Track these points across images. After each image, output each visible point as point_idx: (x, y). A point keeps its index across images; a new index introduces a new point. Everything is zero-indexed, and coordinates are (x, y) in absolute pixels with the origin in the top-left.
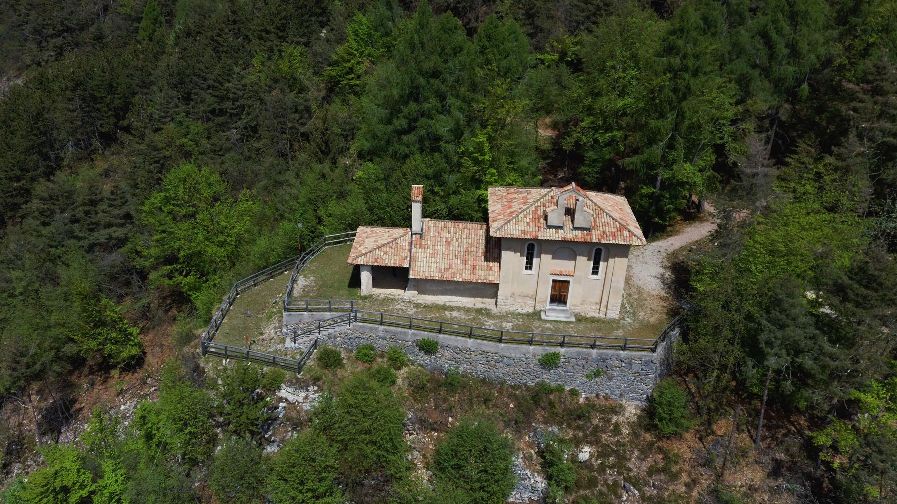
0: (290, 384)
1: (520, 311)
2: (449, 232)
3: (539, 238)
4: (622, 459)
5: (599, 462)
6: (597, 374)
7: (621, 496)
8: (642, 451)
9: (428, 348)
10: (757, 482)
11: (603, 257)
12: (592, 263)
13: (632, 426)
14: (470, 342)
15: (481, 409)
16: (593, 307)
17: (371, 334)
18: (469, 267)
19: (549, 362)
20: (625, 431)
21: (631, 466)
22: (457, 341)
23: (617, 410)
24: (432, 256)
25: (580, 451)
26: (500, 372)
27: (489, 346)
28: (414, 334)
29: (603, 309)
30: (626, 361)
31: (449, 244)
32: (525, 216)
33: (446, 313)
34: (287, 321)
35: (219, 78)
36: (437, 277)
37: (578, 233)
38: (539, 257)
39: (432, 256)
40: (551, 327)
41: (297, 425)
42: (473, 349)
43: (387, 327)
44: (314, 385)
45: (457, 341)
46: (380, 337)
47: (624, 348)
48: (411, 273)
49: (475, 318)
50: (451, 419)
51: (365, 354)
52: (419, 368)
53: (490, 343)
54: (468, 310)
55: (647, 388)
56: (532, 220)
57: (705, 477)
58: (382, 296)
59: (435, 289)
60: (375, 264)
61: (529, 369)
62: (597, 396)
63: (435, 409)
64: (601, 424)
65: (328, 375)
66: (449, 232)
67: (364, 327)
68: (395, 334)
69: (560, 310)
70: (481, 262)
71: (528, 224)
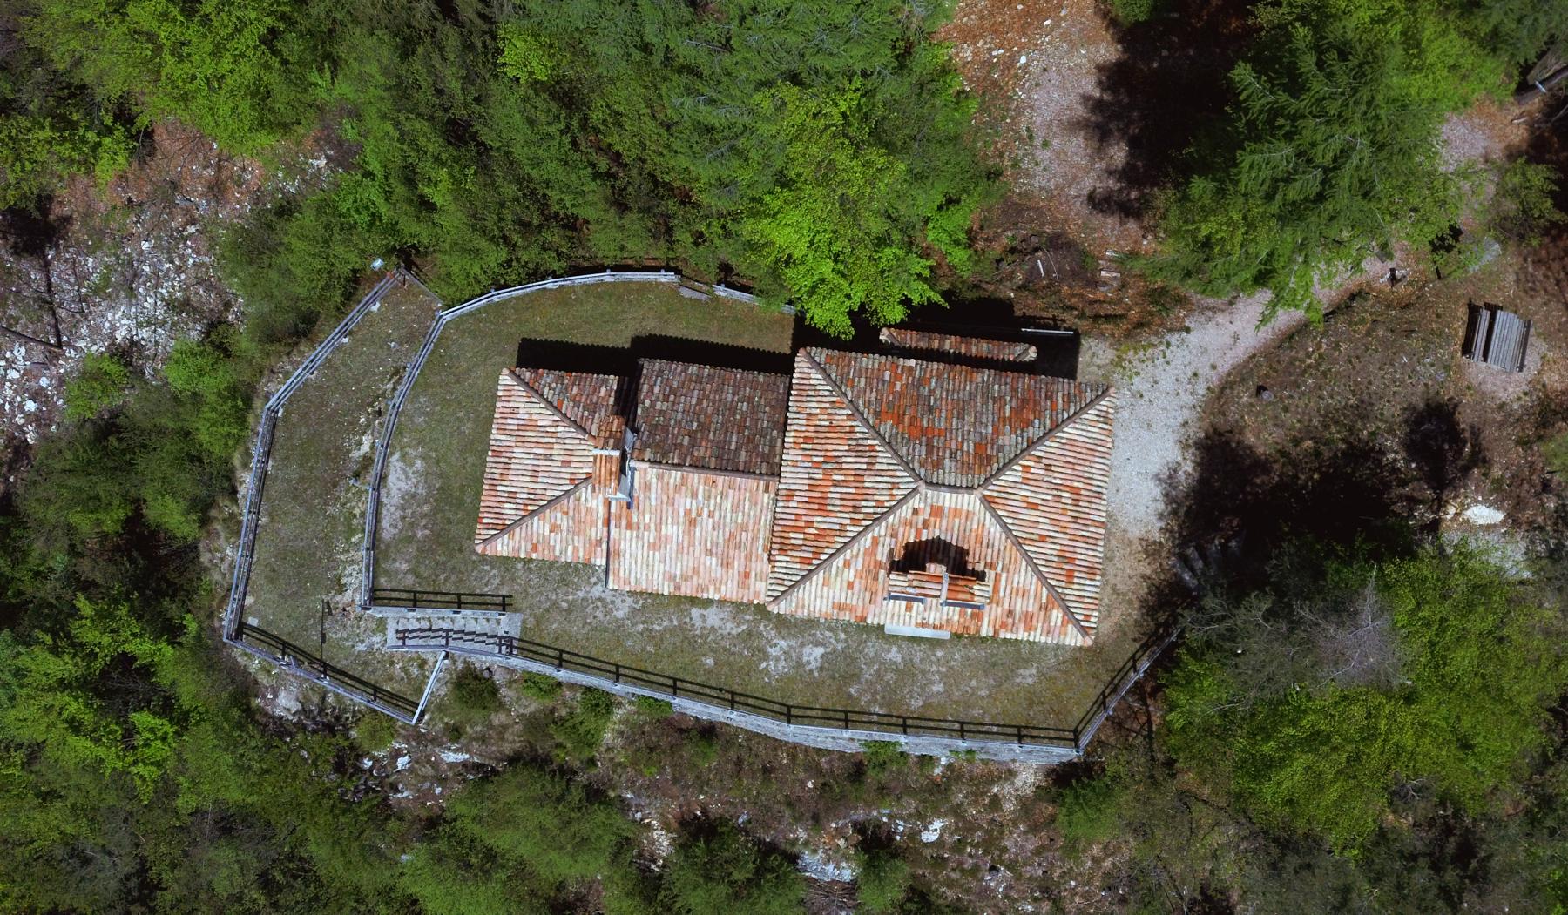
2: (694, 495)
5: (957, 837)
21: (1008, 843)
24: (654, 546)
25: (926, 828)
31: (692, 523)
32: (847, 564)
39: (654, 546)
49: (749, 634)
56: (859, 575)
66: (694, 495)
71: (850, 586)
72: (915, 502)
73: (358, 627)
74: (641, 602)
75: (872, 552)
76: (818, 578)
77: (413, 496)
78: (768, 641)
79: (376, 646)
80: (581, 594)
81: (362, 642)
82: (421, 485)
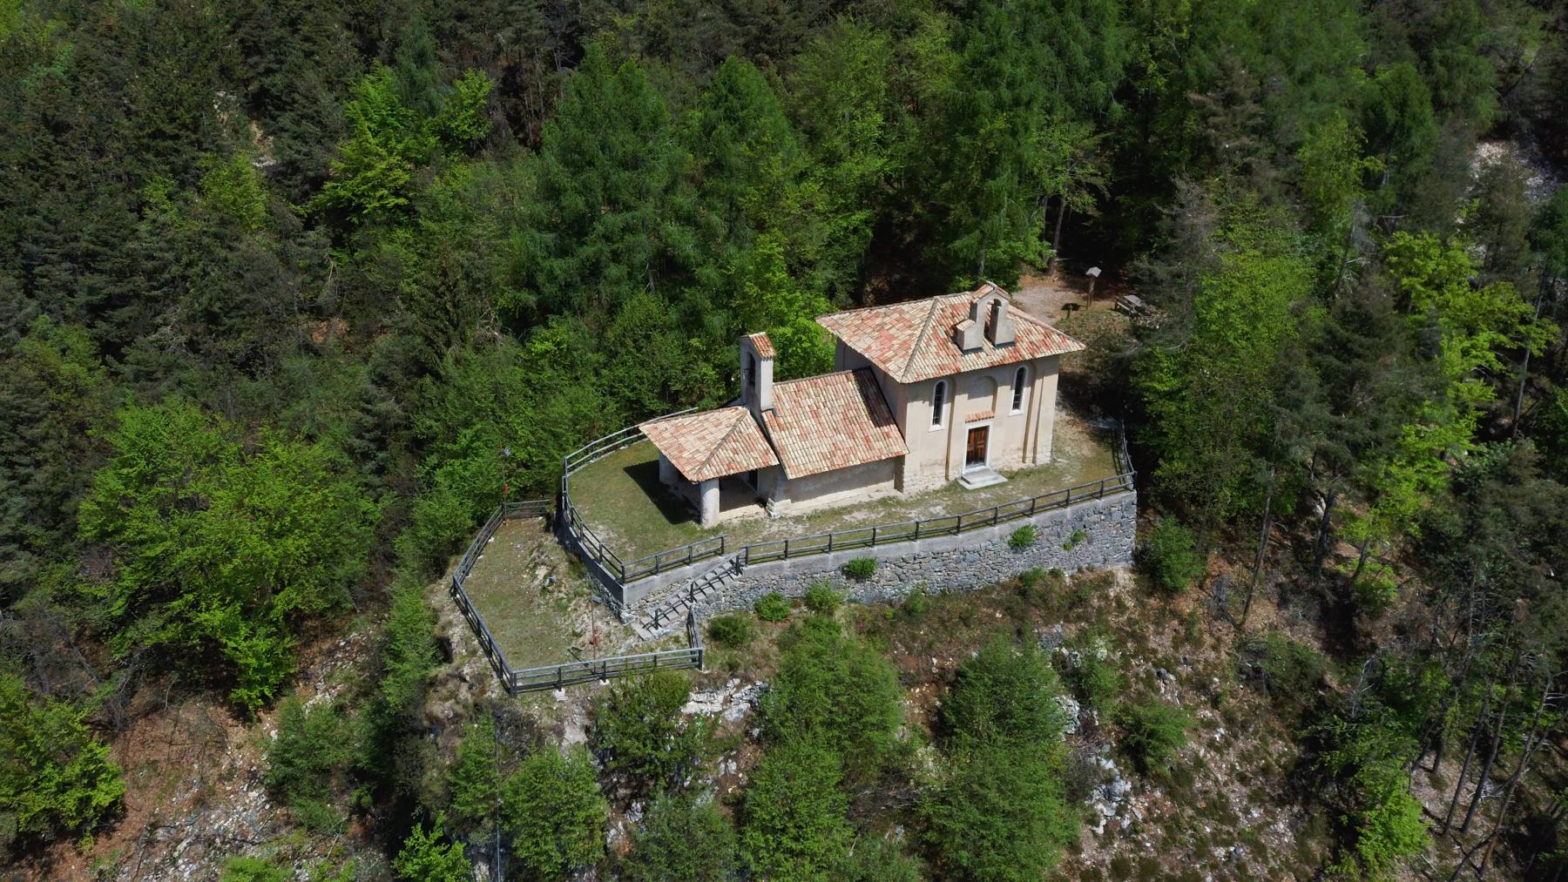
0: (701, 688)
1: (931, 488)
4: (1140, 639)
7: (1159, 689)
8: (1157, 624)
9: (858, 572)
10: (1273, 618)
11: (1026, 379)
13: (1133, 594)
14: (918, 546)
15: (964, 634)
18: (860, 441)
19: (1019, 542)
20: (1130, 603)
22: (900, 548)
23: (1107, 581)
26: (964, 576)
27: (942, 543)
28: (795, 566)
29: (1029, 454)
31: (816, 414)
32: (928, 345)
33: (845, 517)
35: (104, 236)
36: (825, 467)
38: (952, 400)
41: (729, 748)
42: (922, 555)
43: (794, 560)
44: (733, 676)
45: (900, 548)
47: (1101, 494)
48: (788, 471)
50: (935, 661)
51: (769, 609)
53: (944, 538)
54: (870, 506)
55: (1129, 542)
57: (1225, 631)
59: (812, 488)
60: (732, 472)
62: (1080, 570)
63: (910, 654)
64: (1103, 603)
67: (761, 569)
68: (809, 565)
69: (979, 472)
70: (872, 430)
72: (939, 306)
75: (935, 334)
76: (918, 358)
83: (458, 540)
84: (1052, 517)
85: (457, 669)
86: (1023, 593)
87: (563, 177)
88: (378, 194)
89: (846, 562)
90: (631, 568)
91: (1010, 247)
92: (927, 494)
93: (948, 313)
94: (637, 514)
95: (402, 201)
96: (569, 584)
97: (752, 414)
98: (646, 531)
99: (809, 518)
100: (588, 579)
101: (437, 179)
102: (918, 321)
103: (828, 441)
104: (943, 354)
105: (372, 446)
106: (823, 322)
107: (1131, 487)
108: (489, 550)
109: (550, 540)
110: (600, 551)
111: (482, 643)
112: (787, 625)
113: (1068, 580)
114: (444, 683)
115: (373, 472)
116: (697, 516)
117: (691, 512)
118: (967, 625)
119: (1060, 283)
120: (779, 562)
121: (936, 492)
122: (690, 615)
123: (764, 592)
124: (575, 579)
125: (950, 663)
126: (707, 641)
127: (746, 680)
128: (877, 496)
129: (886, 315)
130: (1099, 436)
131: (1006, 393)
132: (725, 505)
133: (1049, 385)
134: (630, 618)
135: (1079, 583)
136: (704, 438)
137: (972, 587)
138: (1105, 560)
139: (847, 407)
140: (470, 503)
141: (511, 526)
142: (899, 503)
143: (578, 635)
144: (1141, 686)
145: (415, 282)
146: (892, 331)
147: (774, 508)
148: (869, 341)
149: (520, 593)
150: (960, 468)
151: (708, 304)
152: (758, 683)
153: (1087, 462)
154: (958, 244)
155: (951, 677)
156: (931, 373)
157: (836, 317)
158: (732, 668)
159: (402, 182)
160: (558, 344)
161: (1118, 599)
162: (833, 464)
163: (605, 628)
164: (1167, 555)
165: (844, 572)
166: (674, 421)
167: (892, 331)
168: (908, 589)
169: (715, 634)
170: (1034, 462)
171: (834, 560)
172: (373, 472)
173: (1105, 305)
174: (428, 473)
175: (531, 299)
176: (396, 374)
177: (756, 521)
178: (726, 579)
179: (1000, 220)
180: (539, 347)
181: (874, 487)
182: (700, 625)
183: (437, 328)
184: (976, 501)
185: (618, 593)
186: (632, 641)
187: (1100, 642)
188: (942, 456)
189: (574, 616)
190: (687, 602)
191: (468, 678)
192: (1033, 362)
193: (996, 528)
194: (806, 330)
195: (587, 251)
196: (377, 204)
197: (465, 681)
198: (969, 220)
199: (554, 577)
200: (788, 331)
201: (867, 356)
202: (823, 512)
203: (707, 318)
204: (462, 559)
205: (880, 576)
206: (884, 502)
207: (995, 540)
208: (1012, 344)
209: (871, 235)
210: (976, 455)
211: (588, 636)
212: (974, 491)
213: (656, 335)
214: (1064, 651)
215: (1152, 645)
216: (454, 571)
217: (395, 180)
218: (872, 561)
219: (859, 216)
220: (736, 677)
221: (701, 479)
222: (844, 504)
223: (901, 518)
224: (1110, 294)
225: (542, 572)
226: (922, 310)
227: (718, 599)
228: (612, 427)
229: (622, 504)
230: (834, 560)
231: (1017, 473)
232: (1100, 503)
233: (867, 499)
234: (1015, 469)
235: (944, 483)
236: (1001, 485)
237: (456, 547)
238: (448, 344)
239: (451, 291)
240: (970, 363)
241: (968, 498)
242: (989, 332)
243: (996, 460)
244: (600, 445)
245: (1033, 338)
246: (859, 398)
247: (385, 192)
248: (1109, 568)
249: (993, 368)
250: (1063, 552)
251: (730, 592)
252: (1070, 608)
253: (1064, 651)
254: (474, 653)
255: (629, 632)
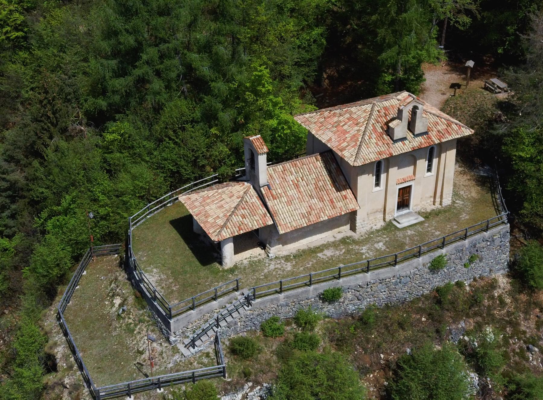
1: (375, 228)
3: (394, 154)
4: (515, 325)
6: (471, 260)
12: (427, 162)
13: (511, 294)
14: (369, 276)
15: (401, 335)
16: (429, 201)
17: (272, 306)
18: (327, 203)
20: (508, 301)
22: (357, 279)
23: (493, 285)
26: (401, 293)
27: (385, 273)
28: (287, 297)
29: (438, 200)
30: (490, 240)
31: (297, 186)
32: (370, 138)
33: (320, 255)
34: (174, 329)
36: (304, 223)
37: (420, 139)
38: (387, 171)
40: (413, 232)
42: (372, 281)
44: (248, 381)
46: (282, 306)
47: (487, 229)
50: (382, 356)
52: (326, 319)
54: (334, 245)
55: (505, 257)
56: (376, 138)
58: (245, 262)
60: (242, 232)
61: (423, 280)
62: (475, 279)
65: (252, 366)
68: (297, 296)
69: (405, 214)
72: (376, 108)
73: (163, 358)
74: (294, 262)
75: (375, 129)
76: (364, 146)
77: (161, 280)
78: (359, 249)
79: (178, 360)
80: (266, 271)
81: (169, 363)
82: (162, 276)
83: (63, 276)
84: (456, 247)
85: (60, 380)
86: (439, 302)
87: (119, 24)
88: (4, 30)
89: (321, 291)
90: (173, 303)
91: (417, 54)
92: (372, 233)
93: (382, 113)
94: (178, 259)
95: (20, 34)
96: (135, 313)
97: (254, 188)
98: (186, 272)
99: (295, 257)
100: (147, 310)
101: (41, 19)
102: (362, 120)
103: (305, 204)
104: (380, 143)
105: (8, 201)
106: (299, 119)
107: (506, 221)
108: (83, 281)
109: (122, 276)
110: (154, 293)
111: (76, 360)
112: (282, 339)
113: (468, 288)
114: (53, 388)
115: (8, 217)
116: (220, 260)
117: (216, 255)
118: (403, 329)
119: (446, 68)
120: (277, 296)
121: (378, 231)
122: (217, 338)
123: (266, 316)
124: (139, 310)
125: (392, 357)
126: (228, 355)
127: (257, 383)
128: (339, 237)
129: (341, 115)
130: (481, 182)
131: (422, 164)
132: (237, 251)
133: (451, 155)
134: (176, 341)
135: (475, 290)
136: (221, 207)
137: (405, 299)
138: (491, 270)
139: (318, 179)
140: (69, 249)
141: (97, 262)
142: (355, 242)
143: (141, 353)
144: (517, 358)
145: (32, 89)
146: (345, 127)
147: (271, 252)
148: (330, 134)
149: (103, 317)
150: (393, 212)
151: (220, 106)
152: (265, 385)
153: (476, 202)
154: (384, 55)
155: (393, 366)
156: (373, 157)
157: (307, 116)
158: (246, 375)
159: (19, 22)
160: (122, 135)
161: (500, 296)
162: (309, 221)
163: (159, 349)
164: (532, 267)
165: (320, 298)
166: (202, 194)
167: (345, 127)
168: (364, 305)
169: (233, 351)
170: (441, 204)
171: (313, 291)
172: (8, 217)
173: (477, 84)
174: (42, 224)
175: (103, 103)
176: (20, 155)
177: (259, 261)
178: (241, 310)
179: (412, 38)
180: (109, 137)
181: (337, 230)
182: (224, 343)
183: (43, 128)
184: (405, 237)
185: (168, 325)
186: (177, 357)
187: (489, 329)
188: (381, 207)
189: (138, 337)
190: (214, 328)
191: (68, 386)
192: (440, 145)
193: (421, 259)
194: (286, 122)
195: (137, 72)
196: (4, 37)
197: (66, 387)
198: (390, 39)
199: (125, 308)
200: (273, 123)
201: (329, 145)
202: (304, 251)
203: (221, 114)
204: (66, 288)
205: (345, 298)
206: (344, 241)
207: (421, 267)
208: (426, 133)
209: (325, 43)
210: (403, 204)
211: (146, 355)
212: (405, 228)
213: (188, 126)
214: (466, 338)
215: (523, 328)
216: (59, 300)
217: (15, 20)
218: (339, 289)
219: (317, 31)
220: (250, 381)
221: (220, 239)
222: (318, 244)
223: (356, 254)
224: (479, 75)
225: (118, 301)
226: (365, 111)
227: (236, 324)
228: (163, 191)
229: (168, 251)
230: (313, 291)
231: (430, 214)
232: (486, 234)
233: (332, 240)
234: (429, 210)
235: (383, 223)
236: (421, 223)
237: (62, 279)
238: (51, 138)
239: (51, 104)
240: (399, 149)
241: (400, 234)
242: (411, 126)
243: (416, 205)
244: (155, 205)
245: (439, 128)
246: (325, 173)
247: (9, 28)
248: (493, 276)
249: (414, 150)
250: (464, 269)
251: (244, 319)
252: (470, 308)
253: (466, 338)
254: (70, 367)
255: (176, 350)
